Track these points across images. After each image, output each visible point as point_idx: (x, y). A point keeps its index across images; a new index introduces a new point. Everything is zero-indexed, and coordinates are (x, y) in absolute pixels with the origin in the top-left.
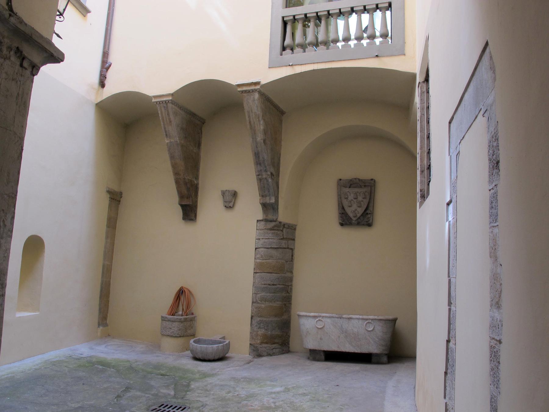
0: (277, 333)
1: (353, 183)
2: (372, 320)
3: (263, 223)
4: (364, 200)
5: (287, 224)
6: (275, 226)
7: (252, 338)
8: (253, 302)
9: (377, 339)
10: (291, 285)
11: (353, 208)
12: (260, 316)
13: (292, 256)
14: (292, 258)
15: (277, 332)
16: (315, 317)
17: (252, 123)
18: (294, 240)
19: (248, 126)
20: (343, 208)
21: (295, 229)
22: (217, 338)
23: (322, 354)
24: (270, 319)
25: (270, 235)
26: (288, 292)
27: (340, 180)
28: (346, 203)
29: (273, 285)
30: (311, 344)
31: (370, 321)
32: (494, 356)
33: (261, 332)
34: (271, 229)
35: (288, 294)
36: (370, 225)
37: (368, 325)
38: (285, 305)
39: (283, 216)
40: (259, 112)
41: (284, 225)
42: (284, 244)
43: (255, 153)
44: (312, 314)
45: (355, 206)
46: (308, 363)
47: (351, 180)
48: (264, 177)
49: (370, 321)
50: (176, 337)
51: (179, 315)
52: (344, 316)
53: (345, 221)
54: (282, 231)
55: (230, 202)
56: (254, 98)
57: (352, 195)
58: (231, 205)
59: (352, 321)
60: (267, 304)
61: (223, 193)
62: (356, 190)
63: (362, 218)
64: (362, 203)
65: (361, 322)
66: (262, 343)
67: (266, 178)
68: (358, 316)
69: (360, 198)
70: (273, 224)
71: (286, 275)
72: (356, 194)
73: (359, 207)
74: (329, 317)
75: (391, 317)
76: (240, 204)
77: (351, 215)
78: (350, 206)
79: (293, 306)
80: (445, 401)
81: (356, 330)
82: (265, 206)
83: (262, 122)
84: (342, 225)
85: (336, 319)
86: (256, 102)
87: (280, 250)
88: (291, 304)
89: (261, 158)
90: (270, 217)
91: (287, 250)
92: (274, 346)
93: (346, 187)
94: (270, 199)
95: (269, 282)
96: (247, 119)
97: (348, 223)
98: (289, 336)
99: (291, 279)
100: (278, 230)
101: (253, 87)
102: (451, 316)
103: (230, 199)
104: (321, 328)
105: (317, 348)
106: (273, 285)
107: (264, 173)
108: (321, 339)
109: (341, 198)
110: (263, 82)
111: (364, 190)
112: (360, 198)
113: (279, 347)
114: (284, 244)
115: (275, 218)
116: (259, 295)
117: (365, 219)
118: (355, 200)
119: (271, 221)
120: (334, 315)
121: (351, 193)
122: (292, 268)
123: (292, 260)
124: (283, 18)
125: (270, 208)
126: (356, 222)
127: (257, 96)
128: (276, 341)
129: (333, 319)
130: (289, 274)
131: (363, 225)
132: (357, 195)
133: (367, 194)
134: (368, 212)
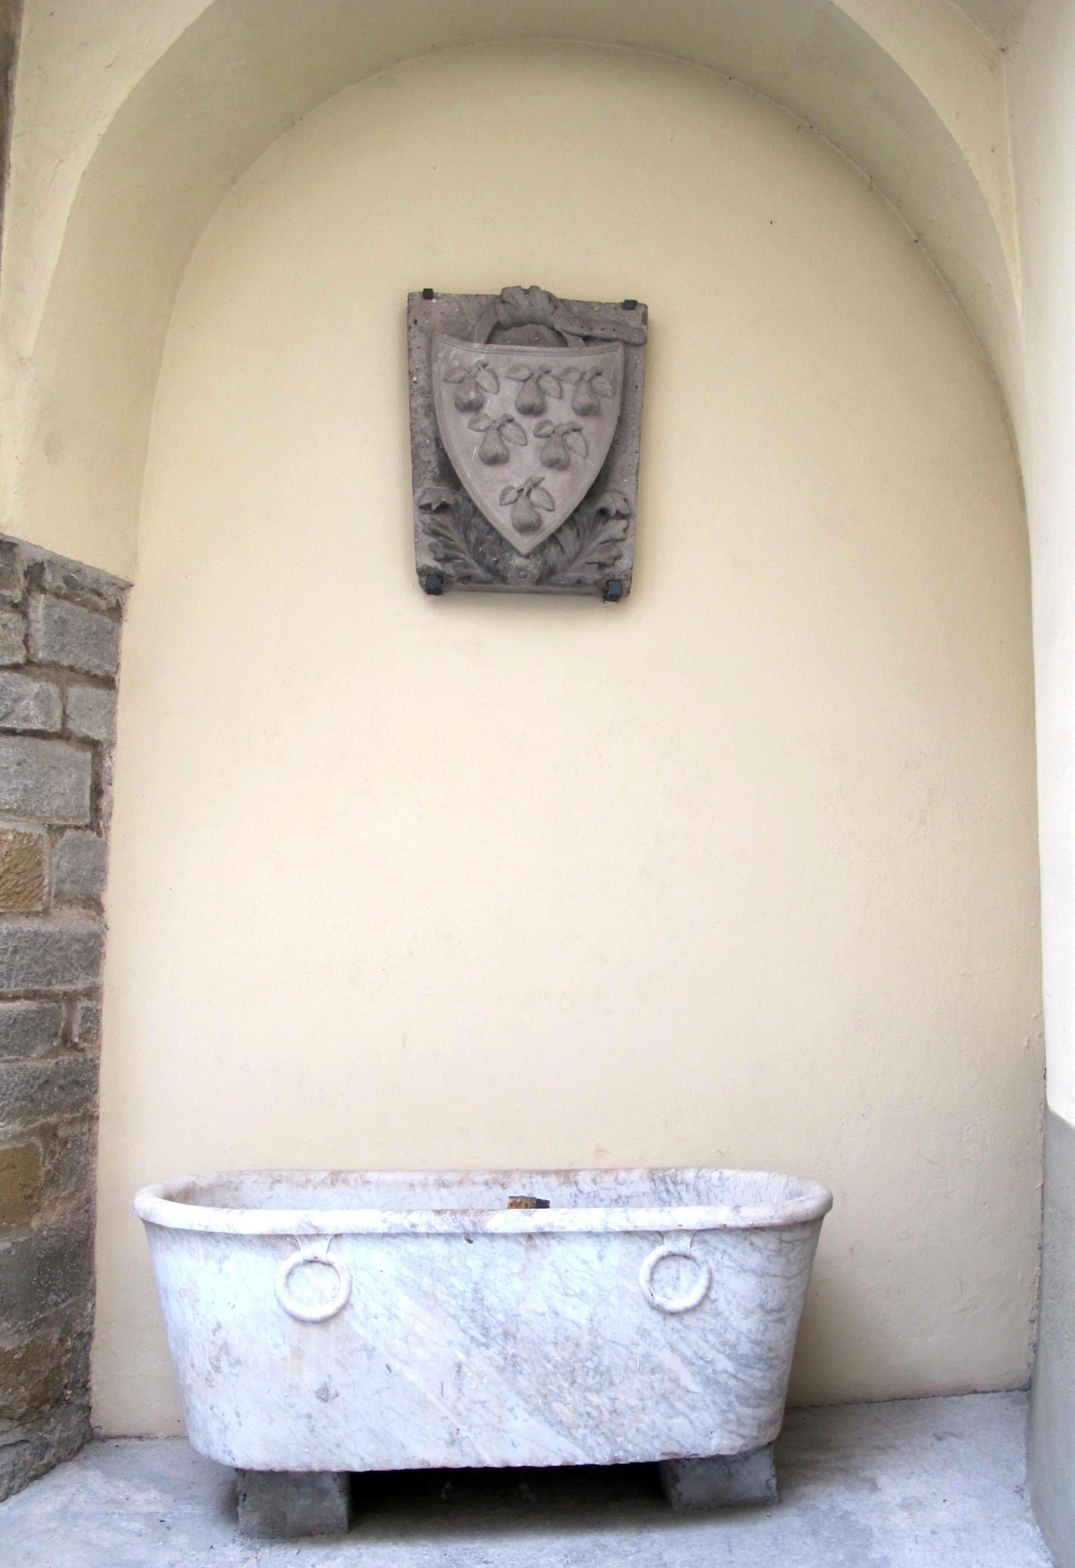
1: (514, 318)
2: (697, 1234)
4: (589, 425)
5: (56, 563)
9: (724, 1364)
10: (93, 993)
13: (97, 791)
14: (96, 810)
16: (273, 1241)
18: (108, 683)
20: (448, 474)
21: (116, 612)
26: (66, 1038)
27: (428, 294)
28: (464, 440)
30: (252, 1433)
31: (683, 1244)
35: (66, 1058)
36: (613, 591)
37: (665, 1273)
38: (49, 1133)
41: (35, 573)
45: (525, 463)
47: (502, 299)
49: (683, 1244)
54: (20, 608)
57: (510, 390)
59: (557, 1250)
62: (535, 357)
63: (569, 538)
64: (572, 439)
65: (615, 1251)
69: (560, 413)
71: (48, 927)
73: (555, 464)
77: (502, 518)
78: (495, 461)
79: (105, 1131)
81: (578, 1314)
84: (434, 585)
85: (438, 1247)
88: (91, 1118)
91: (61, 749)
93: (468, 338)
97: (479, 572)
98: (86, 1337)
99: (90, 953)
104: (323, 1322)
105: (294, 1457)
109: (430, 410)
111: (585, 360)
112: (560, 413)
113: (17, 1435)
117: (586, 557)
118: (529, 423)
120: (423, 1220)
121: (501, 378)
122: (98, 873)
123: (95, 817)
129: (413, 1247)
130: (70, 921)
132: (541, 392)
133: (603, 384)
134: (611, 501)
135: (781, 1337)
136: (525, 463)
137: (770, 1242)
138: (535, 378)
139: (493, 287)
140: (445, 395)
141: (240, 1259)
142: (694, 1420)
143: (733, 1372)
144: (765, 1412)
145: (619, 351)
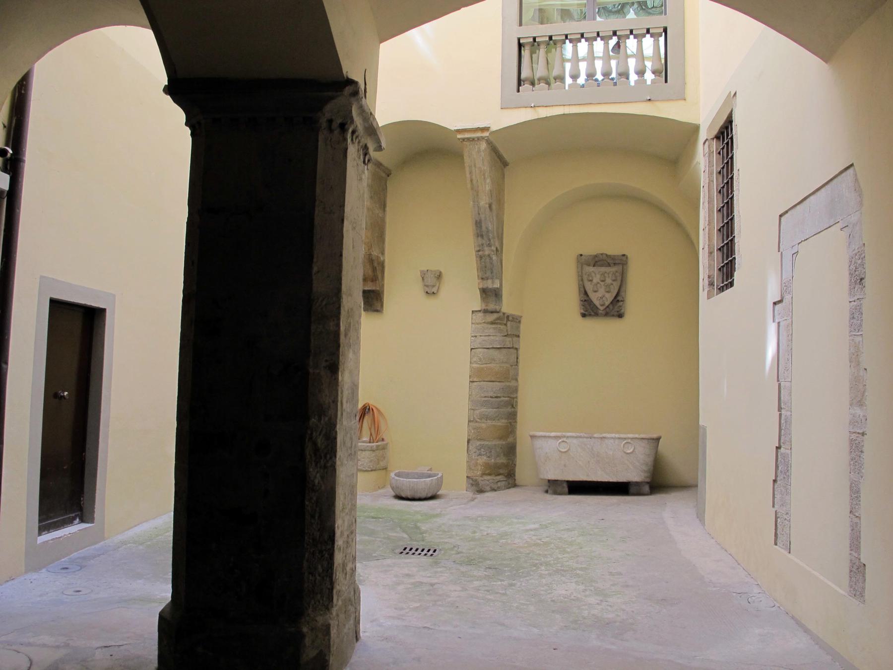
0: (502, 461)
1: (598, 261)
3: (481, 314)
4: (615, 283)
5: (512, 315)
6: (498, 319)
7: (469, 468)
8: (469, 421)
11: (599, 294)
12: (480, 440)
15: (502, 460)
17: (474, 182)
18: (519, 336)
19: (469, 186)
20: (586, 293)
21: (520, 322)
22: (424, 470)
23: (565, 485)
24: (494, 443)
25: (491, 330)
28: (589, 287)
29: (496, 397)
32: (856, 448)
33: (483, 460)
34: (492, 323)
36: (620, 316)
39: (507, 306)
40: (486, 168)
41: (508, 317)
42: (508, 342)
43: (476, 221)
44: (553, 434)
45: (602, 292)
46: (548, 497)
47: (596, 256)
48: (487, 253)
50: (366, 471)
51: (364, 442)
52: (595, 435)
53: (589, 310)
54: (506, 325)
55: (434, 286)
56: (479, 148)
57: (598, 276)
58: (434, 290)
59: (606, 441)
60: (490, 422)
61: (423, 275)
62: (603, 269)
63: (611, 307)
65: (617, 441)
66: (483, 474)
67: (489, 255)
68: (613, 435)
69: (609, 281)
70: (495, 316)
72: (603, 274)
73: (608, 292)
74: (576, 437)
75: (655, 436)
76: (447, 289)
77: (597, 303)
78: (595, 292)
80: (774, 510)
82: (484, 292)
83: (488, 181)
86: (483, 154)
87: (504, 351)
88: (516, 422)
89: (484, 228)
90: (492, 307)
91: (511, 350)
92: (499, 478)
93: (589, 265)
94: (493, 283)
95: (491, 394)
96: (468, 175)
99: (516, 390)
100: (500, 324)
101: (479, 134)
102: (783, 422)
103: (432, 284)
106: (496, 397)
107: (486, 248)
108: (565, 466)
109: (582, 280)
110: (494, 128)
111: (613, 269)
112: (609, 281)
114: (508, 342)
115: (498, 308)
116: (477, 412)
117: (615, 309)
118: (602, 283)
119: (492, 312)
121: (597, 273)
122: (517, 374)
124: (519, 39)
125: (490, 294)
126: (603, 313)
127: (483, 145)
128: (501, 471)
130: (513, 383)
131: (613, 316)
133: (617, 274)
134: (619, 298)
135: (650, 460)
136: (602, 292)
137: (646, 441)
138: (603, 274)
139: (594, 252)
140: (585, 277)
141: (551, 441)
142: (633, 474)
143: (484, 307)
144: (646, 475)
145: (621, 267)
